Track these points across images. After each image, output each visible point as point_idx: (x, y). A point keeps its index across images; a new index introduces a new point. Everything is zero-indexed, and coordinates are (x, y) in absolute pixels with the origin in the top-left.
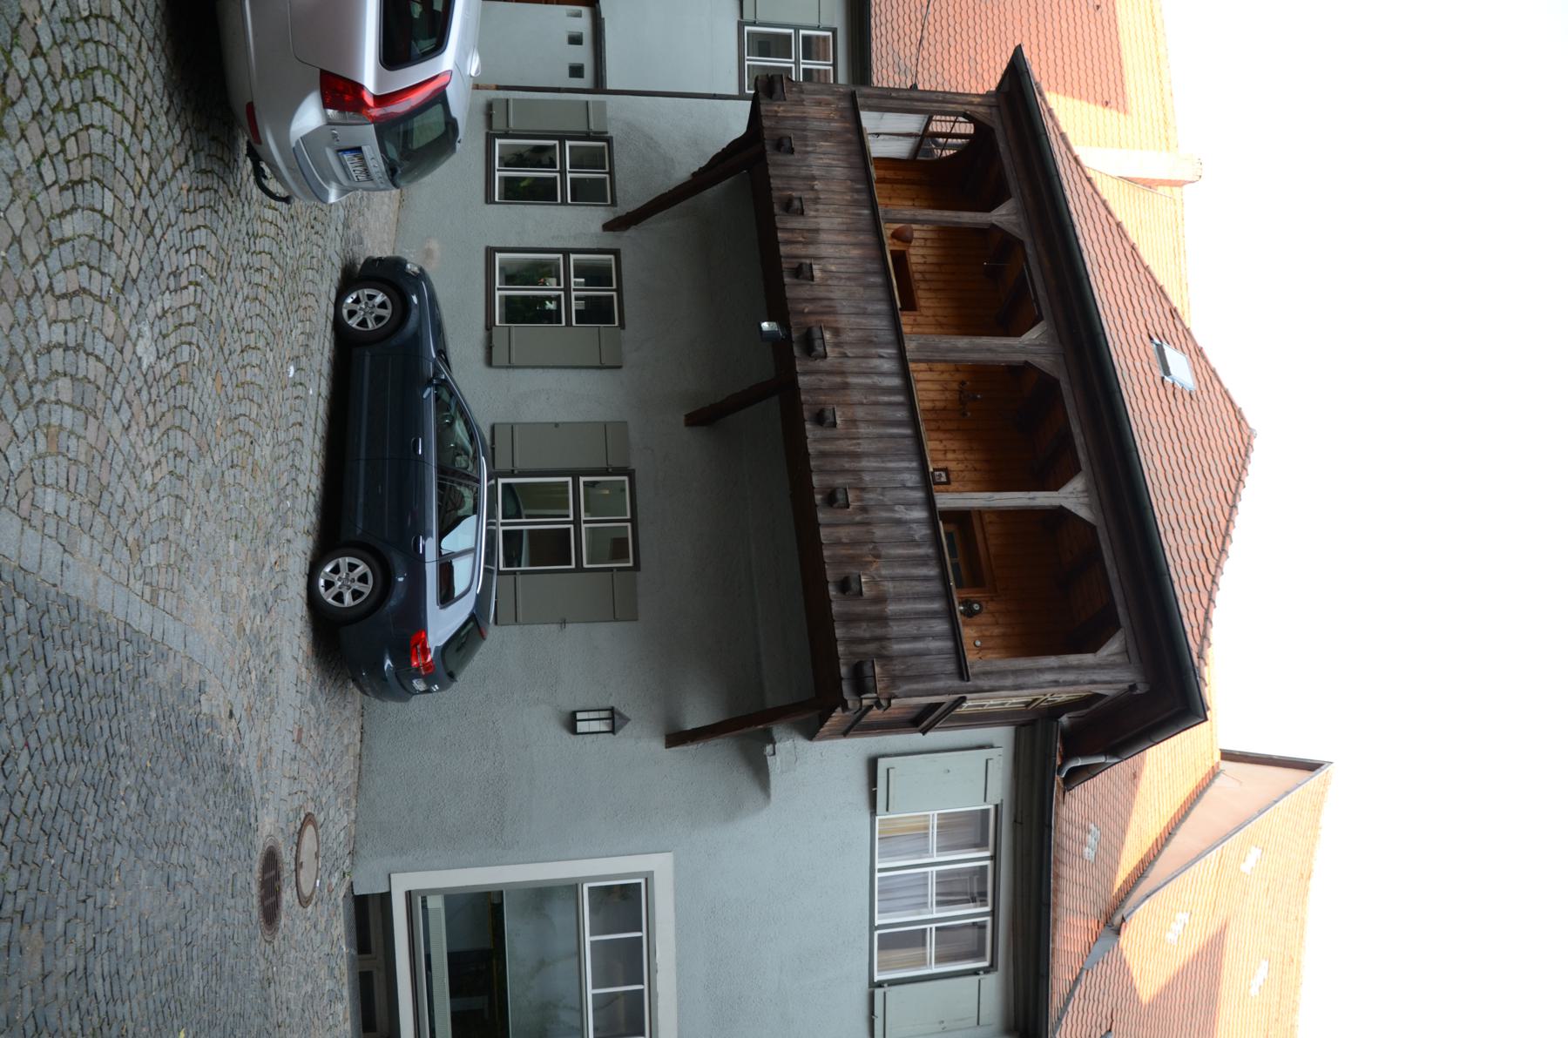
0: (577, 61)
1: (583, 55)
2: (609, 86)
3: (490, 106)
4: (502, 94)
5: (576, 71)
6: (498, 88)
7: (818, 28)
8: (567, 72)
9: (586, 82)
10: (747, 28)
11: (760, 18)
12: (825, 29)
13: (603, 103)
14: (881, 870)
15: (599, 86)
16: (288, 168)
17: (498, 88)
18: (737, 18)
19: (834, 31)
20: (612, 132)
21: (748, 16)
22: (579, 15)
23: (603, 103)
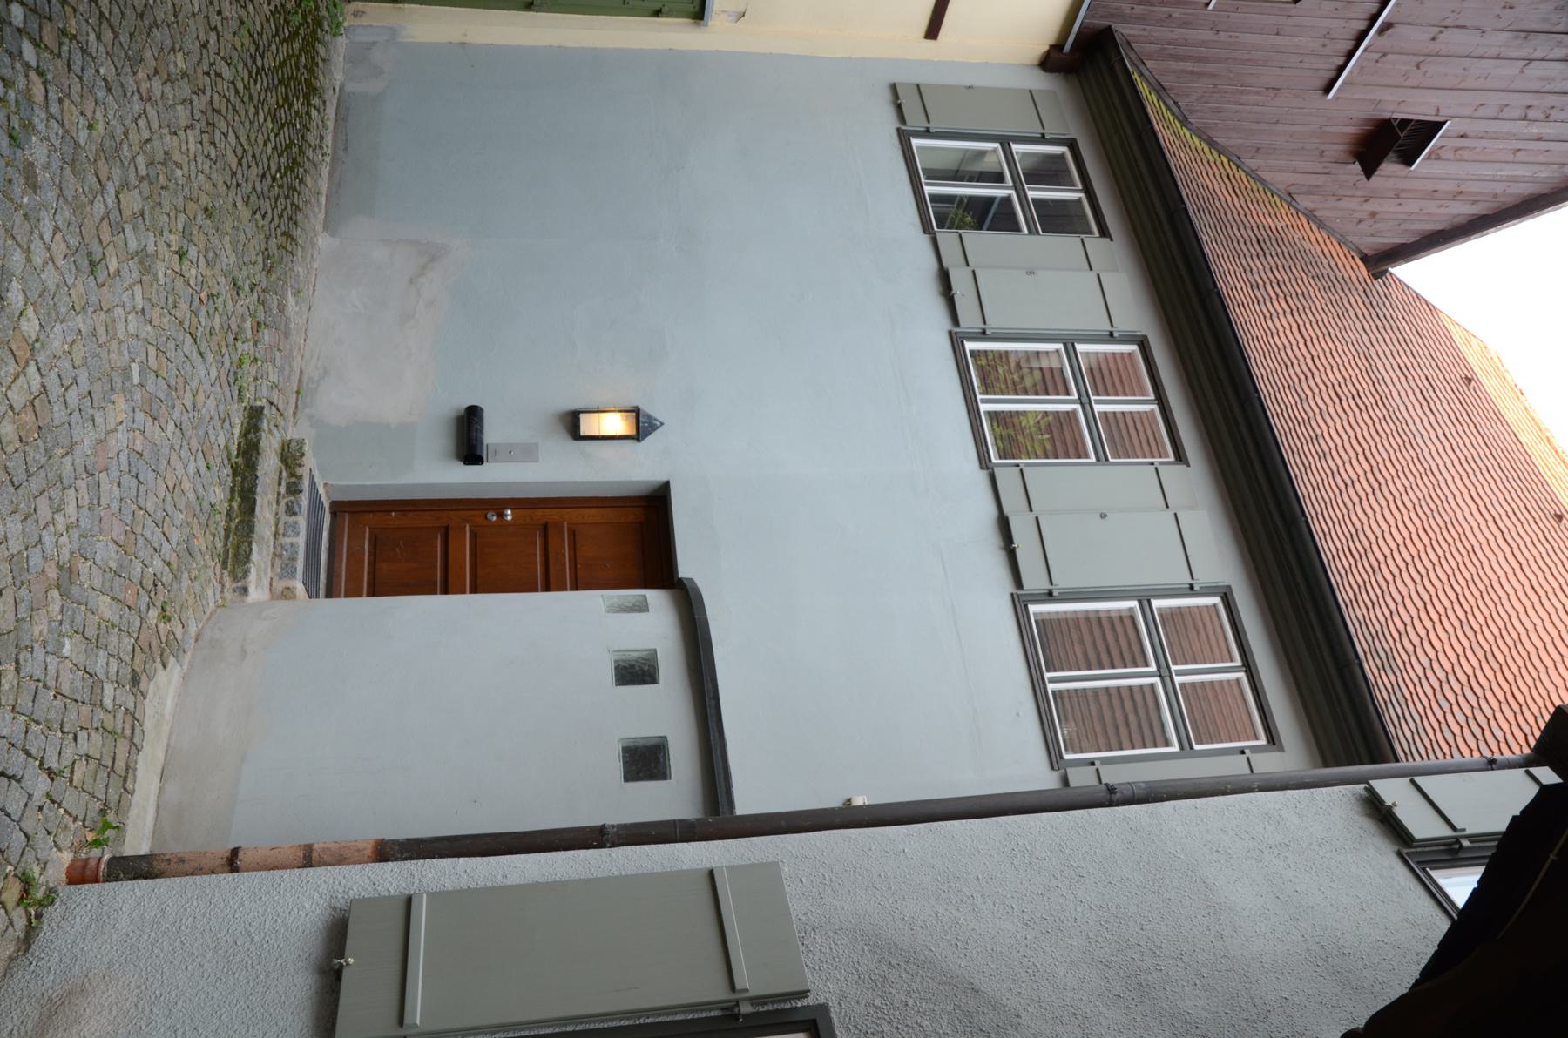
0: (644, 729)
1: (662, 711)
2: (747, 802)
3: (338, 932)
4: (394, 878)
5: (645, 761)
6: (385, 852)
7: (1191, 590)
8: (617, 767)
9: (673, 798)
10: (1033, 608)
11: (1062, 582)
12: (1207, 591)
13: (770, 871)
14: (1053, 680)
15: (717, 817)
16: (777, 1011)
17: (385, 852)
18: (1007, 586)
19: (1227, 598)
20: (823, 989)
21: (1033, 579)
22: (642, 607)
23: (770, 871)
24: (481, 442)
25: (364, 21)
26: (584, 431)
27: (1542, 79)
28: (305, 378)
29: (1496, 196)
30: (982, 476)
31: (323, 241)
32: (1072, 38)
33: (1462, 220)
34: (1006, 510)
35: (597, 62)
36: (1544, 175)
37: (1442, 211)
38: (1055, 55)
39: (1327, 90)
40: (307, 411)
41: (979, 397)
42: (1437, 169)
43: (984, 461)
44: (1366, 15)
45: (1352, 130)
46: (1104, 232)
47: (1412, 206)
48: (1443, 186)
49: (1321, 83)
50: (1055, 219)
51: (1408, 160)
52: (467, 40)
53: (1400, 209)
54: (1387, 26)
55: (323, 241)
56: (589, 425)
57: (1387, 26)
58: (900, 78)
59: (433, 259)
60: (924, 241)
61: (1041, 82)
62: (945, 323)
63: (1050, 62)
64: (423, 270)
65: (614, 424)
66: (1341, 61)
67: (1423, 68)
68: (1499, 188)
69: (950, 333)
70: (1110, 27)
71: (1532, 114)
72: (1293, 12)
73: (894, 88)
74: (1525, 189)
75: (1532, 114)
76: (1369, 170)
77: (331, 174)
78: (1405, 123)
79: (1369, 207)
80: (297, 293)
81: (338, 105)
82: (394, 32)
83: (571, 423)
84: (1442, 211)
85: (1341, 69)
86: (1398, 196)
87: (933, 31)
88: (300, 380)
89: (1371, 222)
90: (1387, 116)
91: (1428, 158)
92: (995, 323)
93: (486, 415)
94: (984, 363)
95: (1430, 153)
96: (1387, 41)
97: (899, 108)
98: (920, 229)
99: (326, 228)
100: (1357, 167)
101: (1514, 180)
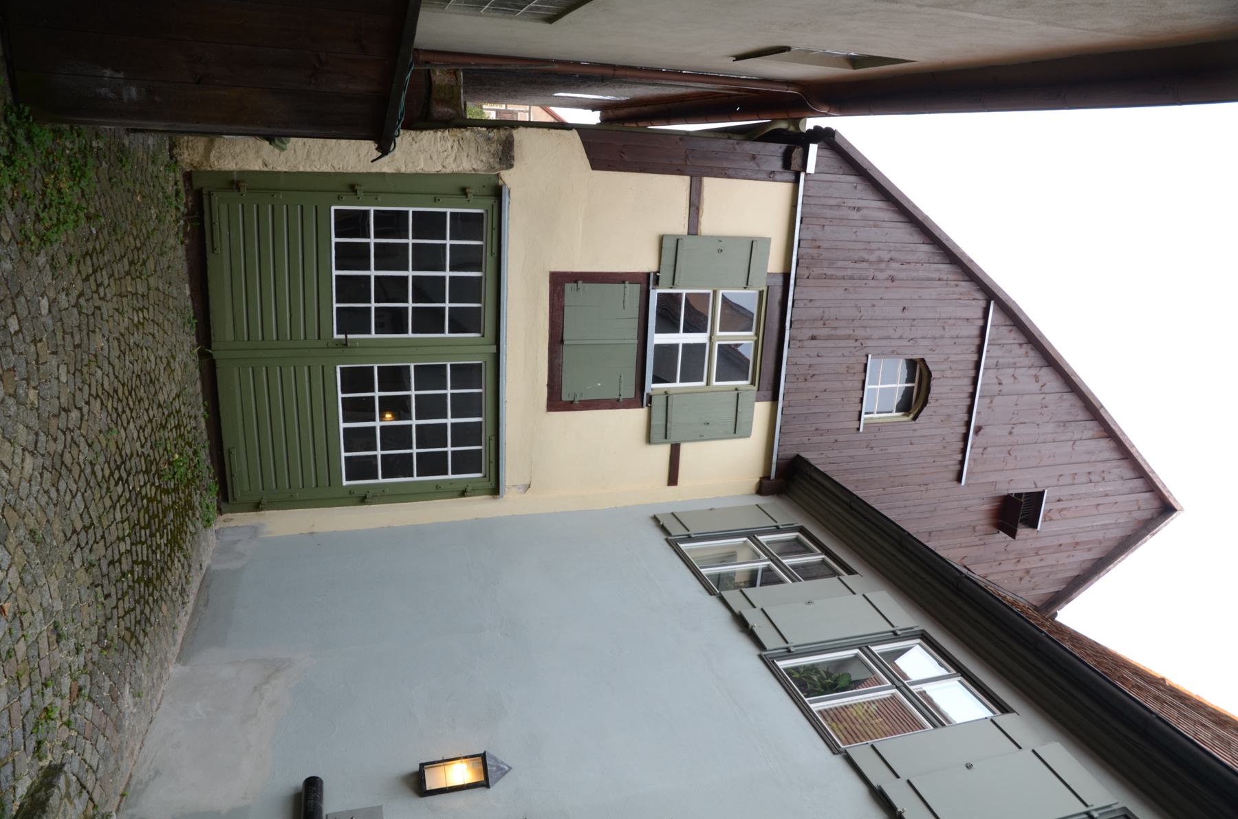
24: (321, 810)
25: (232, 524)
26: (431, 785)
27: (1088, 453)
28: (133, 782)
29: (1100, 542)
30: (838, 761)
31: (174, 670)
32: (774, 467)
33: (1087, 565)
34: (875, 783)
35: (420, 532)
36: (1122, 521)
37: (1071, 560)
38: (765, 482)
39: (959, 479)
40: (130, 811)
41: (806, 700)
42: (1054, 527)
43: (834, 749)
44: (962, 423)
45: (987, 507)
46: (850, 572)
47: (1051, 559)
48: (1065, 540)
49: (953, 475)
50: (807, 573)
51: (1033, 524)
52: (315, 530)
53: (1043, 564)
54: (978, 430)
55: (174, 670)
56: (434, 780)
57: (978, 430)
58: (657, 512)
59: (278, 670)
60: (713, 601)
61: (761, 500)
62: (753, 651)
63: (763, 488)
64: (267, 680)
65: (460, 773)
66: (959, 457)
67: (1013, 454)
68: (1099, 535)
69: (760, 656)
70: (798, 456)
71: (1093, 478)
72: (916, 427)
73: (655, 519)
74: (1116, 534)
75: (1093, 478)
76: (1013, 534)
77: (190, 623)
78: (1019, 495)
79: (1021, 566)
80: (136, 695)
81: (204, 578)
82: (255, 530)
83: (417, 784)
84: (1071, 560)
85: (962, 463)
86: (1037, 554)
87: (673, 479)
88: (128, 784)
89: (1028, 578)
90: (1005, 493)
91: (1044, 520)
92: (794, 640)
93: (326, 787)
94: (797, 675)
95: (1045, 516)
96: (981, 439)
97: (663, 528)
98: (706, 594)
99: (179, 659)
100: (1002, 535)
101: (1105, 527)
